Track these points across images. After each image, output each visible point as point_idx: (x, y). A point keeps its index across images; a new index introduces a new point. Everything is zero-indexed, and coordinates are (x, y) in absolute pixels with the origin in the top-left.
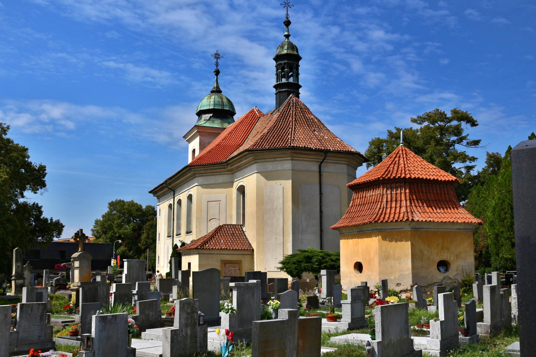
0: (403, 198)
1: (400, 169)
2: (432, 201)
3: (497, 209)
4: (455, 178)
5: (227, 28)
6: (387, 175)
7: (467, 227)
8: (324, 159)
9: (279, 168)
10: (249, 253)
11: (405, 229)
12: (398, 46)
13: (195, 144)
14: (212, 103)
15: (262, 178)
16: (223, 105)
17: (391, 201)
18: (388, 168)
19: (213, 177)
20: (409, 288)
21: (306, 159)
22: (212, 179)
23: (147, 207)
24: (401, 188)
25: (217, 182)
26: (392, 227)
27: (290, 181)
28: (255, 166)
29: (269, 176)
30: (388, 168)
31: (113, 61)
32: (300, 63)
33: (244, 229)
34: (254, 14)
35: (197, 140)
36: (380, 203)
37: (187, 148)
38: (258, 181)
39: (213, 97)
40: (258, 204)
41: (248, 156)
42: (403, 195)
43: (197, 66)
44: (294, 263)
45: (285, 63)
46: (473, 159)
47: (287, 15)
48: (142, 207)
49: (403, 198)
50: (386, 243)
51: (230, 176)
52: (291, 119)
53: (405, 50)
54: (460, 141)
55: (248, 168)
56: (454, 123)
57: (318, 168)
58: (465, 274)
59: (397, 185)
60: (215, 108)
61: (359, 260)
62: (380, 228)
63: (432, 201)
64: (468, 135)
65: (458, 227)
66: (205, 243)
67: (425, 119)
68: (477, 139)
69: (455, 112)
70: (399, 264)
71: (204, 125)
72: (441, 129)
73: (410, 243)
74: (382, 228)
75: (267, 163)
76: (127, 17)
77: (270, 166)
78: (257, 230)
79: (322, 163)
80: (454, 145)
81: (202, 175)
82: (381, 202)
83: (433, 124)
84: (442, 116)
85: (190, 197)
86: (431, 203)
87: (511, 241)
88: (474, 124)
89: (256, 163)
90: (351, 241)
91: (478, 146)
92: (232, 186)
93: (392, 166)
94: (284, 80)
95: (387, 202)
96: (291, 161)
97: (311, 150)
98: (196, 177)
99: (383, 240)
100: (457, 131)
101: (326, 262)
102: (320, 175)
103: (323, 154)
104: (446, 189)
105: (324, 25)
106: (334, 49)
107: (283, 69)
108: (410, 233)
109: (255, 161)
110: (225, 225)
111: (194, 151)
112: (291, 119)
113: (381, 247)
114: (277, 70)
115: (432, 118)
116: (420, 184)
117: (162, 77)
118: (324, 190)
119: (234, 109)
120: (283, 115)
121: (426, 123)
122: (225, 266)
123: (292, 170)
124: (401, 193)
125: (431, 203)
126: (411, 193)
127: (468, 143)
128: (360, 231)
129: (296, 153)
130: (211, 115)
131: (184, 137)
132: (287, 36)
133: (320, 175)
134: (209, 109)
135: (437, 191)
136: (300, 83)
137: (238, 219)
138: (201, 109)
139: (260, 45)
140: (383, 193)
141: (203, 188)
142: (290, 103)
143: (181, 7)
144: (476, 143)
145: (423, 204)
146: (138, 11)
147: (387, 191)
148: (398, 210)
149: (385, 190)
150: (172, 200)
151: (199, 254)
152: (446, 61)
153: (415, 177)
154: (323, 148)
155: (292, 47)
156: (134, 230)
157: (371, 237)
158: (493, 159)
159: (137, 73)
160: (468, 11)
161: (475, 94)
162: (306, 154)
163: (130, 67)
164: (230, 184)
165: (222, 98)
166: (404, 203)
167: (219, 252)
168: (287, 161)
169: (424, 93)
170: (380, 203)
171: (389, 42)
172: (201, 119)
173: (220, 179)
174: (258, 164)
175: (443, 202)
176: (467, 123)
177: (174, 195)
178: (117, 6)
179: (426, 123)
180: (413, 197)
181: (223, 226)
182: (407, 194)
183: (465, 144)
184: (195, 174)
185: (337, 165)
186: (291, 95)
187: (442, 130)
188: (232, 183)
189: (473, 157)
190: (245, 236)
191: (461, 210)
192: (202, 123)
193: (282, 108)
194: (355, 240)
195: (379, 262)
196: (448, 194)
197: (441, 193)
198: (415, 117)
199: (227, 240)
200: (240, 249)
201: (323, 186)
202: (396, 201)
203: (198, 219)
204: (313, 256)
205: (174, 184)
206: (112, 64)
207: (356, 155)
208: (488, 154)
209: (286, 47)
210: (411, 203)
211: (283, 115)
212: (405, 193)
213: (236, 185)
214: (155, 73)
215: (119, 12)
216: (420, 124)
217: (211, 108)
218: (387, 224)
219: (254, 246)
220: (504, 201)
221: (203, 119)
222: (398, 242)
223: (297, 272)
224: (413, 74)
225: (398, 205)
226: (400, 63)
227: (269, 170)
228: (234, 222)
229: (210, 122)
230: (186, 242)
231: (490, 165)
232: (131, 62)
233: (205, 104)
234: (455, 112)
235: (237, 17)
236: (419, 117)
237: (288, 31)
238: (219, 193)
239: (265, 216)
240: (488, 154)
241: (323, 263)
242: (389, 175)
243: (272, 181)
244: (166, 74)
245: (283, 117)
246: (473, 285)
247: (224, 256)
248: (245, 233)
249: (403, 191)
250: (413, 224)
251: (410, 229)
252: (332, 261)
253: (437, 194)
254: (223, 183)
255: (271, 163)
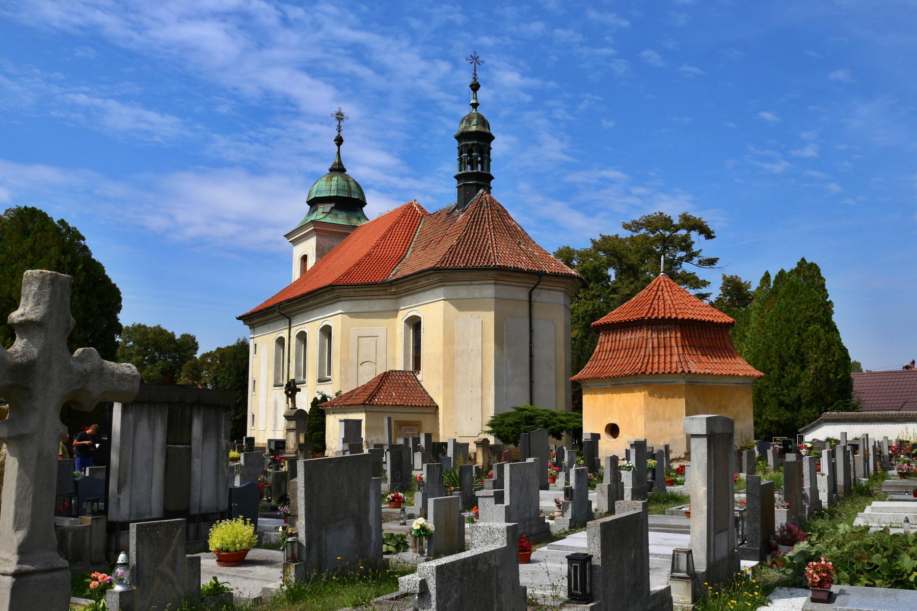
0: (674, 344)
1: (668, 307)
5: (275, 53)
6: (653, 314)
7: (747, 381)
8: (538, 283)
10: (430, 410)
12: (539, 98)
13: (309, 247)
14: (333, 187)
18: (652, 304)
19: (367, 302)
22: (365, 305)
24: (665, 331)
25: (372, 310)
26: (662, 380)
28: (440, 292)
29: (461, 305)
30: (652, 304)
31: (85, 93)
32: (493, 144)
33: (419, 377)
34: (320, 35)
35: (312, 243)
36: (643, 349)
38: (445, 312)
40: (445, 344)
41: (431, 277)
42: (673, 340)
43: (223, 109)
46: (705, 284)
49: (674, 344)
52: (487, 226)
53: (550, 103)
54: (690, 257)
55: (428, 293)
56: (683, 232)
64: (701, 250)
65: (736, 381)
66: (373, 396)
67: (642, 224)
70: (670, 426)
71: (324, 220)
76: (113, 25)
77: (463, 291)
79: (533, 288)
83: (653, 233)
84: (666, 223)
85: (326, 331)
88: (709, 235)
90: (600, 397)
92: (396, 316)
94: (469, 169)
95: (653, 348)
97: (521, 271)
100: (686, 245)
101: (554, 424)
105: (426, 57)
106: (441, 95)
107: (470, 152)
109: (442, 283)
111: (304, 258)
112: (487, 226)
114: (460, 154)
115: (652, 223)
117: (164, 125)
119: (364, 198)
126: (682, 337)
127: (700, 261)
128: (618, 383)
132: (475, 106)
134: (330, 197)
136: (491, 173)
139: (327, 83)
143: (202, 16)
144: (711, 262)
146: (132, 17)
151: (366, 412)
155: (483, 122)
156: (163, 372)
157: (633, 392)
159: (122, 117)
160: (645, 53)
163: (112, 104)
164: (394, 313)
165: (348, 181)
166: (675, 350)
167: (378, 409)
170: (643, 349)
177: (290, 324)
178: (97, 7)
179: (643, 231)
182: (679, 339)
183: (696, 263)
185: (552, 292)
186: (481, 191)
187: (664, 241)
193: (470, 206)
194: (607, 396)
198: (628, 222)
201: (534, 321)
202: (665, 347)
206: (82, 99)
208: (724, 277)
209: (474, 121)
210: (683, 350)
212: (676, 338)
214: (153, 116)
215: (99, 17)
216: (636, 231)
219: (439, 401)
220: (770, 347)
224: (561, 140)
225: (668, 353)
226: (542, 122)
230: (327, 394)
231: (726, 292)
232: (116, 98)
233: (323, 188)
235: (292, 37)
236: (635, 222)
238: (376, 326)
239: (458, 361)
240: (724, 277)
244: (171, 120)
245: (475, 222)
247: (399, 415)
248: (422, 383)
249: (673, 335)
250: (689, 376)
252: (562, 422)
254: (382, 311)
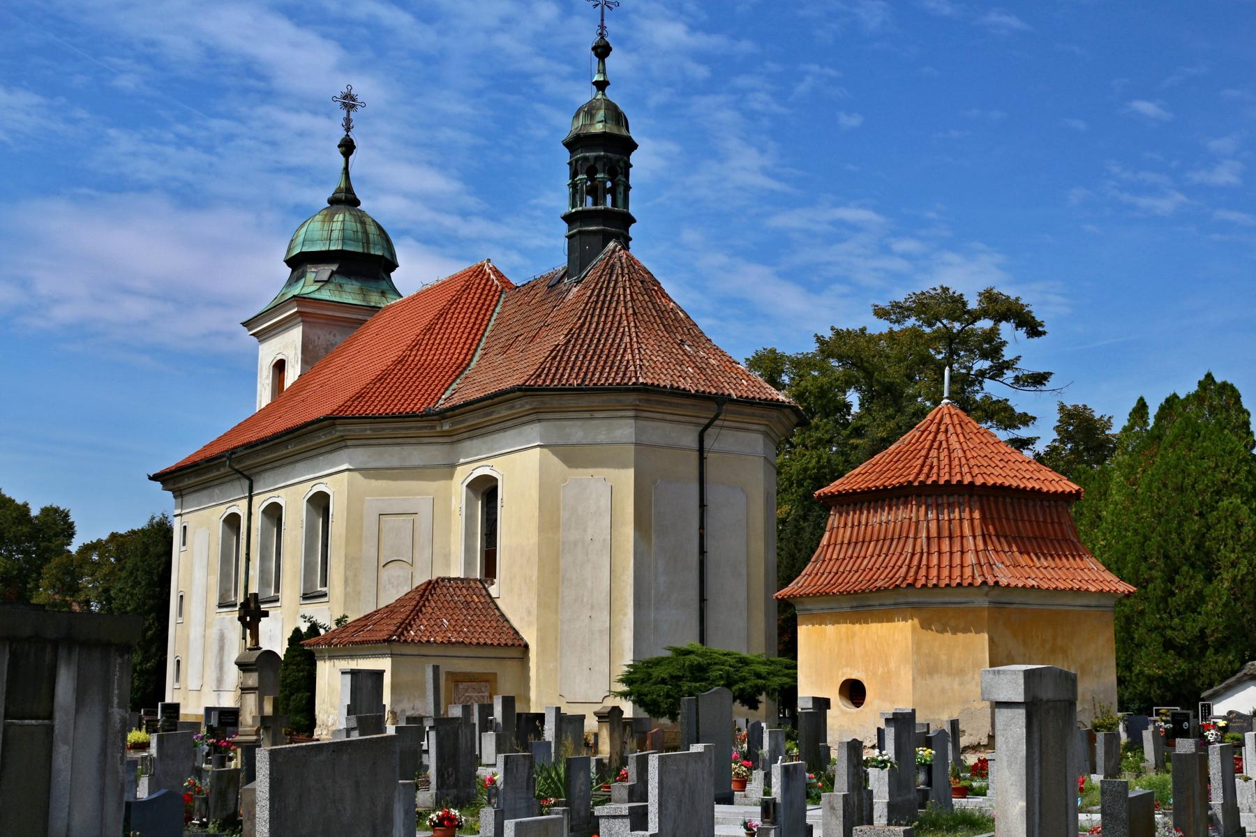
0: (967, 531)
2: (1029, 538)
3: (1129, 558)
4: (1076, 487)
8: (716, 418)
9: (602, 437)
10: (516, 653)
11: (976, 605)
13: (289, 345)
14: (335, 234)
15: (555, 461)
16: (368, 242)
17: (939, 537)
18: (926, 457)
20: (985, 741)
21: (669, 417)
22: (393, 456)
23: (47, 511)
25: (407, 464)
26: (946, 599)
27: (631, 472)
28: (534, 432)
29: (571, 455)
30: (926, 457)
32: (634, 158)
35: (295, 335)
36: (911, 541)
37: (255, 357)
39: (341, 217)
40: (541, 529)
42: (966, 524)
44: (663, 681)
45: (597, 158)
46: (1026, 420)
47: (602, 27)
48: (28, 510)
49: (967, 531)
50: (929, 635)
51: (446, 447)
52: (621, 309)
53: (742, 81)
54: (998, 371)
56: (985, 324)
57: (697, 439)
58: (1098, 710)
59: (951, 500)
60: (347, 248)
61: (855, 676)
62: (915, 600)
63: (1029, 538)
64: (1018, 358)
66: (405, 626)
67: (909, 309)
68: (1042, 371)
69: (989, 297)
70: (961, 684)
72: (950, 339)
73: (986, 636)
74: (922, 599)
75: (570, 423)
77: (576, 431)
78: (539, 596)
80: (981, 383)
81: (364, 441)
82: (915, 539)
83: (930, 325)
84: (954, 306)
85: (320, 503)
86: (1027, 543)
87: (1163, 636)
88: (1034, 329)
89: (539, 420)
90: (830, 630)
91: (1043, 388)
92: (451, 476)
93: (934, 453)
94: (589, 204)
95: (928, 538)
96: (632, 421)
97: (685, 394)
98: (346, 447)
99: (922, 627)
100: (991, 347)
101: (744, 680)
102: (702, 459)
103: (714, 406)
104: (1054, 510)
107: (591, 172)
108: (986, 614)
109: (536, 415)
110: (443, 579)
111: (280, 366)
113: (917, 645)
115: (925, 307)
116: (1008, 500)
118: (710, 498)
119: (393, 255)
120: (598, 296)
121: (911, 322)
122: (457, 686)
123: (636, 444)
124: (961, 519)
125: (1027, 543)
127: (1017, 379)
128: (862, 604)
129: (648, 401)
130: (334, 268)
131: (245, 324)
132: (601, 86)
133: (702, 459)
134: (329, 252)
135: (1036, 516)
137: (468, 563)
138: (305, 249)
140: (918, 517)
141: (366, 477)
142: (613, 265)
144: (1038, 379)
145: (1010, 547)
147: (926, 514)
148: (957, 560)
149: (923, 509)
150: (245, 502)
151: (392, 655)
152: (854, 121)
153: (984, 484)
154: (714, 391)
155: (616, 116)
157: (890, 620)
158: (1076, 422)
161: (931, 215)
162: (670, 404)
165: (363, 223)
167: (441, 651)
168: (622, 422)
169: (788, 203)
171: (701, 57)
172: (303, 276)
173: (416, 455)
174: (544, 424)
175: (1051, 541)
176: (1018, 326)
180: (988, 529)
181: (437, 581)
182: (977, 522)
184: (343, 439)
185: (741, 434)
186: (611, 245)
188: (453, 466)
189: (1026, 414)
190: (498, 608)
191: (1090, 562)
192: (306, 287)
194: (844, 628)
195: (914, 680)
196: (1060, 523)
197: (1045, 522)
198: (884, 304)
199: (451, 623)
200: (496, 642)
202: (951, 537)
203: (350, 562)
204: (709, 664)
205: (248, 463)
207: (787, 411)
208: (1062, 408)
209: (601, 115)
211: (598, 296)
212: (972, 520)
213: (465, 474)
217: (333, 248)
218: (936, 590)
219: (530, 636)
221: (310, 276)
222: (960, 634)
223: (672, 704)
224: (762, 151)
225: (957, 547)
226: (727, 116)
227: (574, 441)
228: (457, 572)
229: (331, 286)
234: (989, 297)
236: (896, 305)
237: (604, 74)
239: (566, 560)
240: (1062, 408)
241: (736, 682)
242: (922, 478)
243: (580, 470)
246: (1145, 733)
247: (455, 661)
249: (966, 515)
251: (986, 605)
252: (758, 676)
253: (1038, 522)
255: (579, 423)
